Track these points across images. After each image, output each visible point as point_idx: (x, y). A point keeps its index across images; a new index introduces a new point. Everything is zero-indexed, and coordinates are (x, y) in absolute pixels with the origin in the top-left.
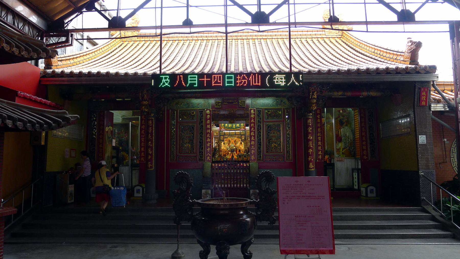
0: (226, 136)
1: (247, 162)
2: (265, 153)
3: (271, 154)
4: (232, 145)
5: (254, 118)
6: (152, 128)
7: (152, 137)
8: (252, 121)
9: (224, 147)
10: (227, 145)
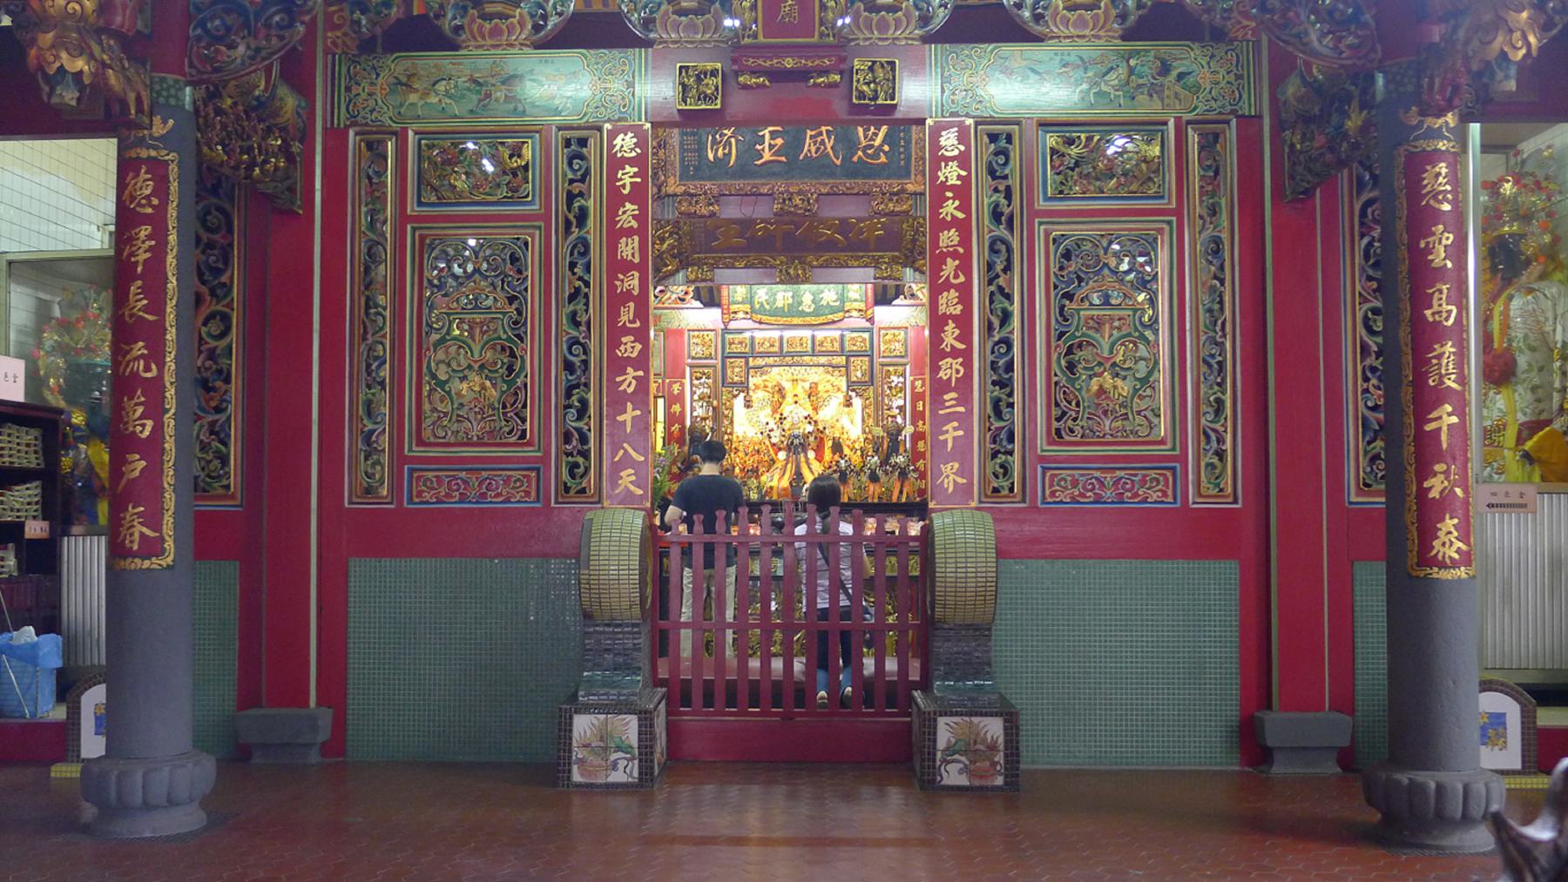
0: (760, 362)
1: (918, 509)
2: (1041, 440)
3: (1081, 451)
4: (796, 412)
5: (962, 192)
6: (160, 234)
7: (157, 306)
8: (950, 208)
9: (748, 424)
10: (765, 415)
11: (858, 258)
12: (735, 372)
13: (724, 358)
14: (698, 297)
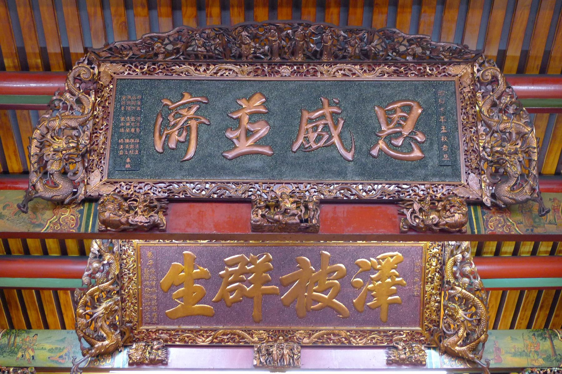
11: (363, 335)
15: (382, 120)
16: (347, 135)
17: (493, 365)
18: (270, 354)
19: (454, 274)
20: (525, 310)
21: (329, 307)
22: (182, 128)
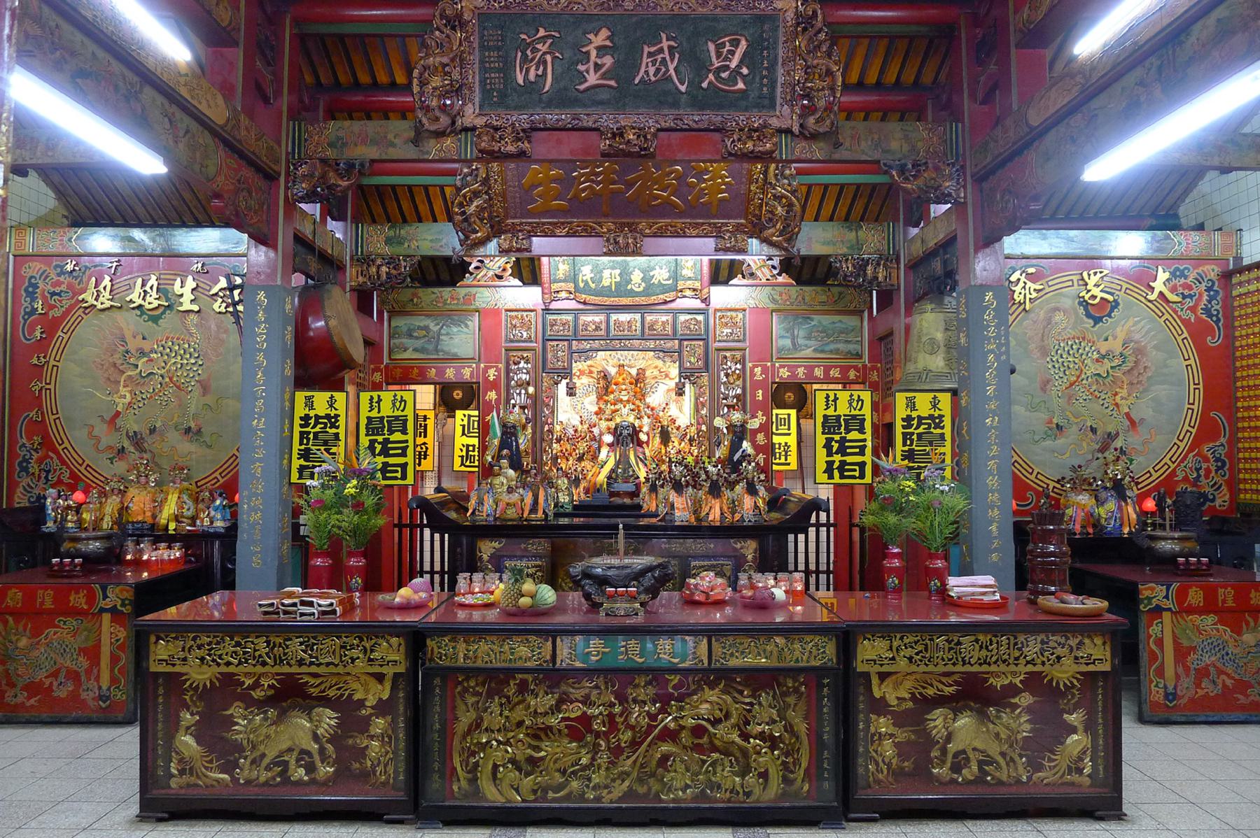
9: (572, 410)
10: (590, 403)
11: (697, 226)
12: (558, 353)
13: (545, 340)
14: (518, 272)
15: (713, 54)
16: (682, 69)
17: (803, 252)
18: (616, 243)
19: (776, 175)
20: (845, 198)
21: (667, 203)
22: (539, 62)
